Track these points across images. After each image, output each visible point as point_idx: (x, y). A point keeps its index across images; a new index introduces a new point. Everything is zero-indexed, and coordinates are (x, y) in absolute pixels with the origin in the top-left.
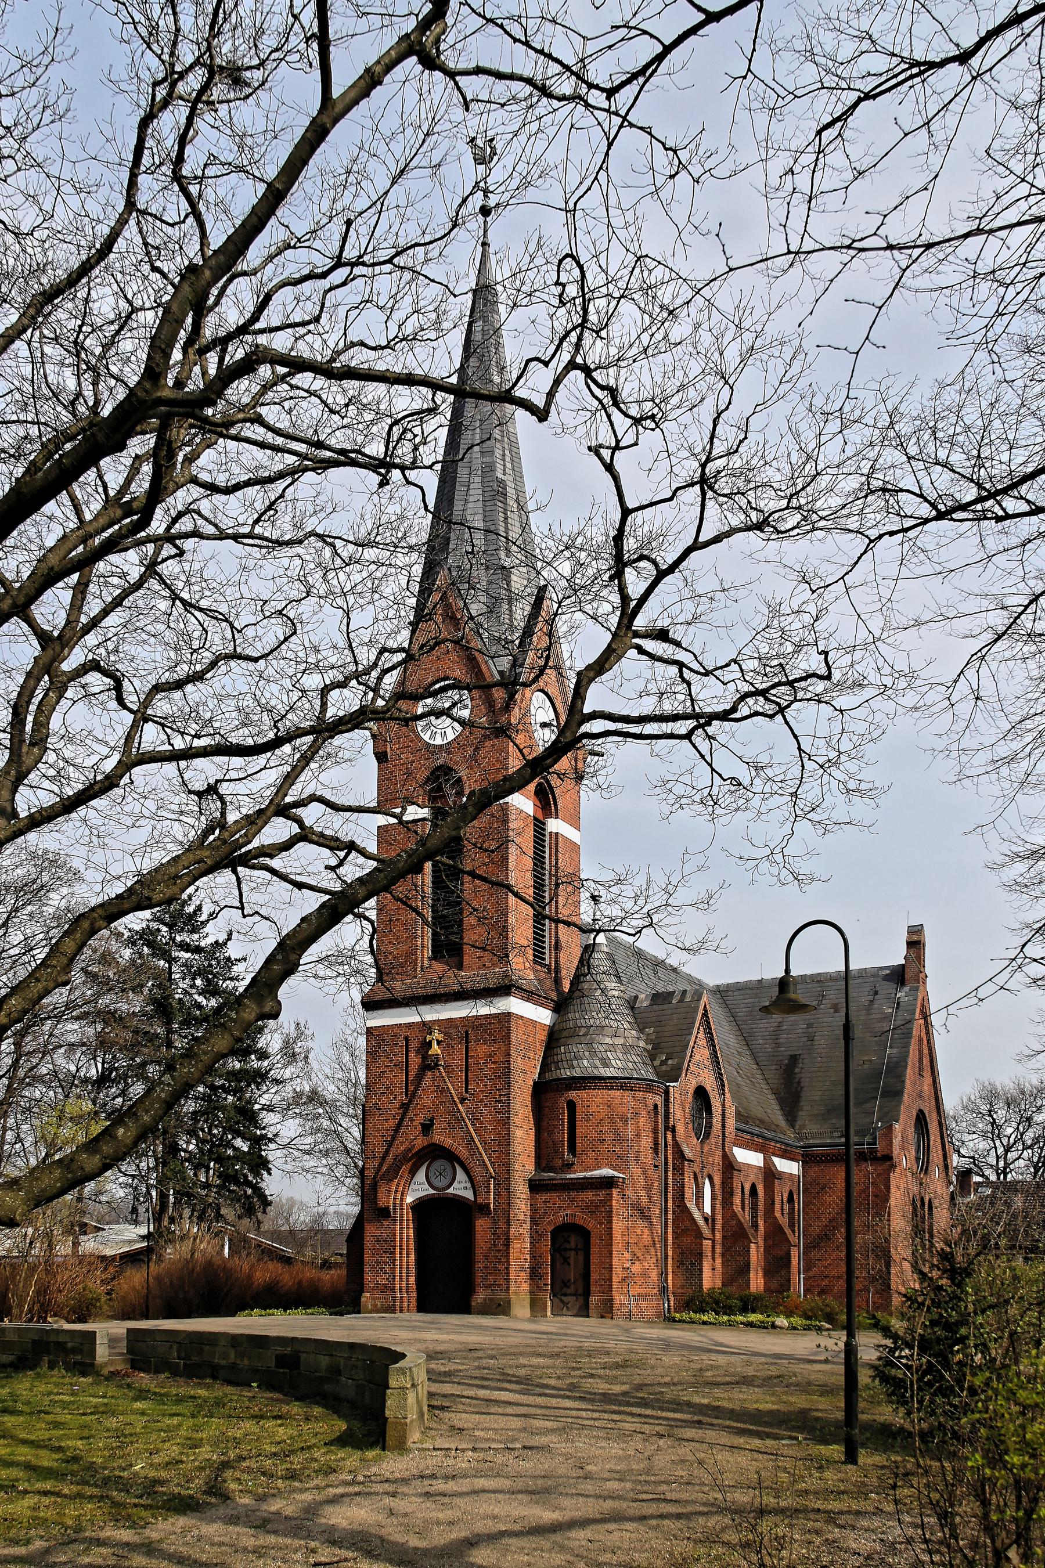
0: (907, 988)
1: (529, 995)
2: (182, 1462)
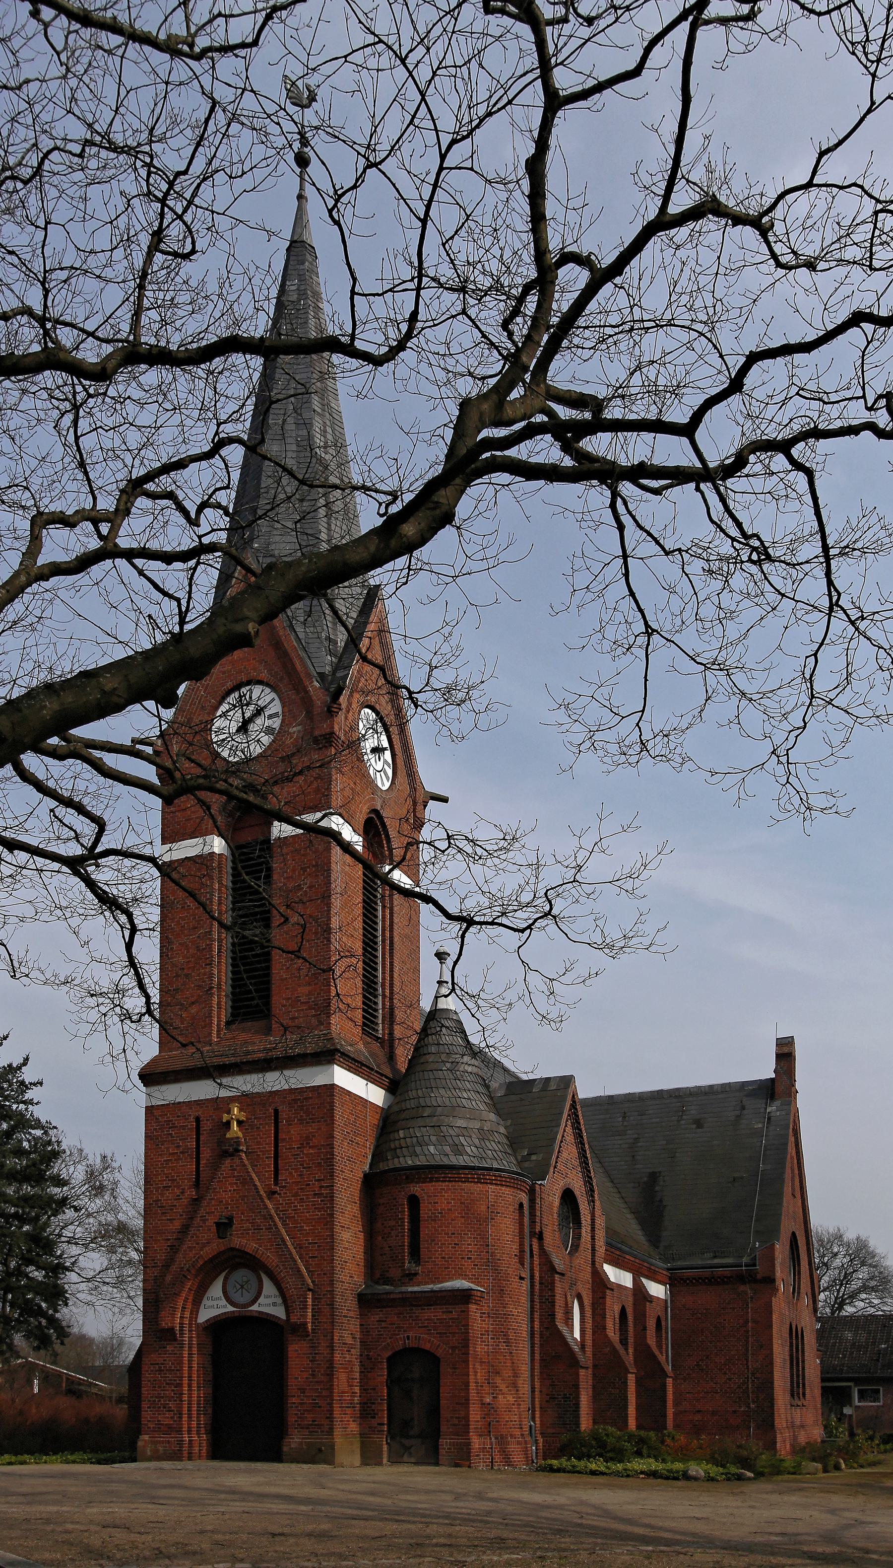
0: (778, 1103)
1: (357, 1067)
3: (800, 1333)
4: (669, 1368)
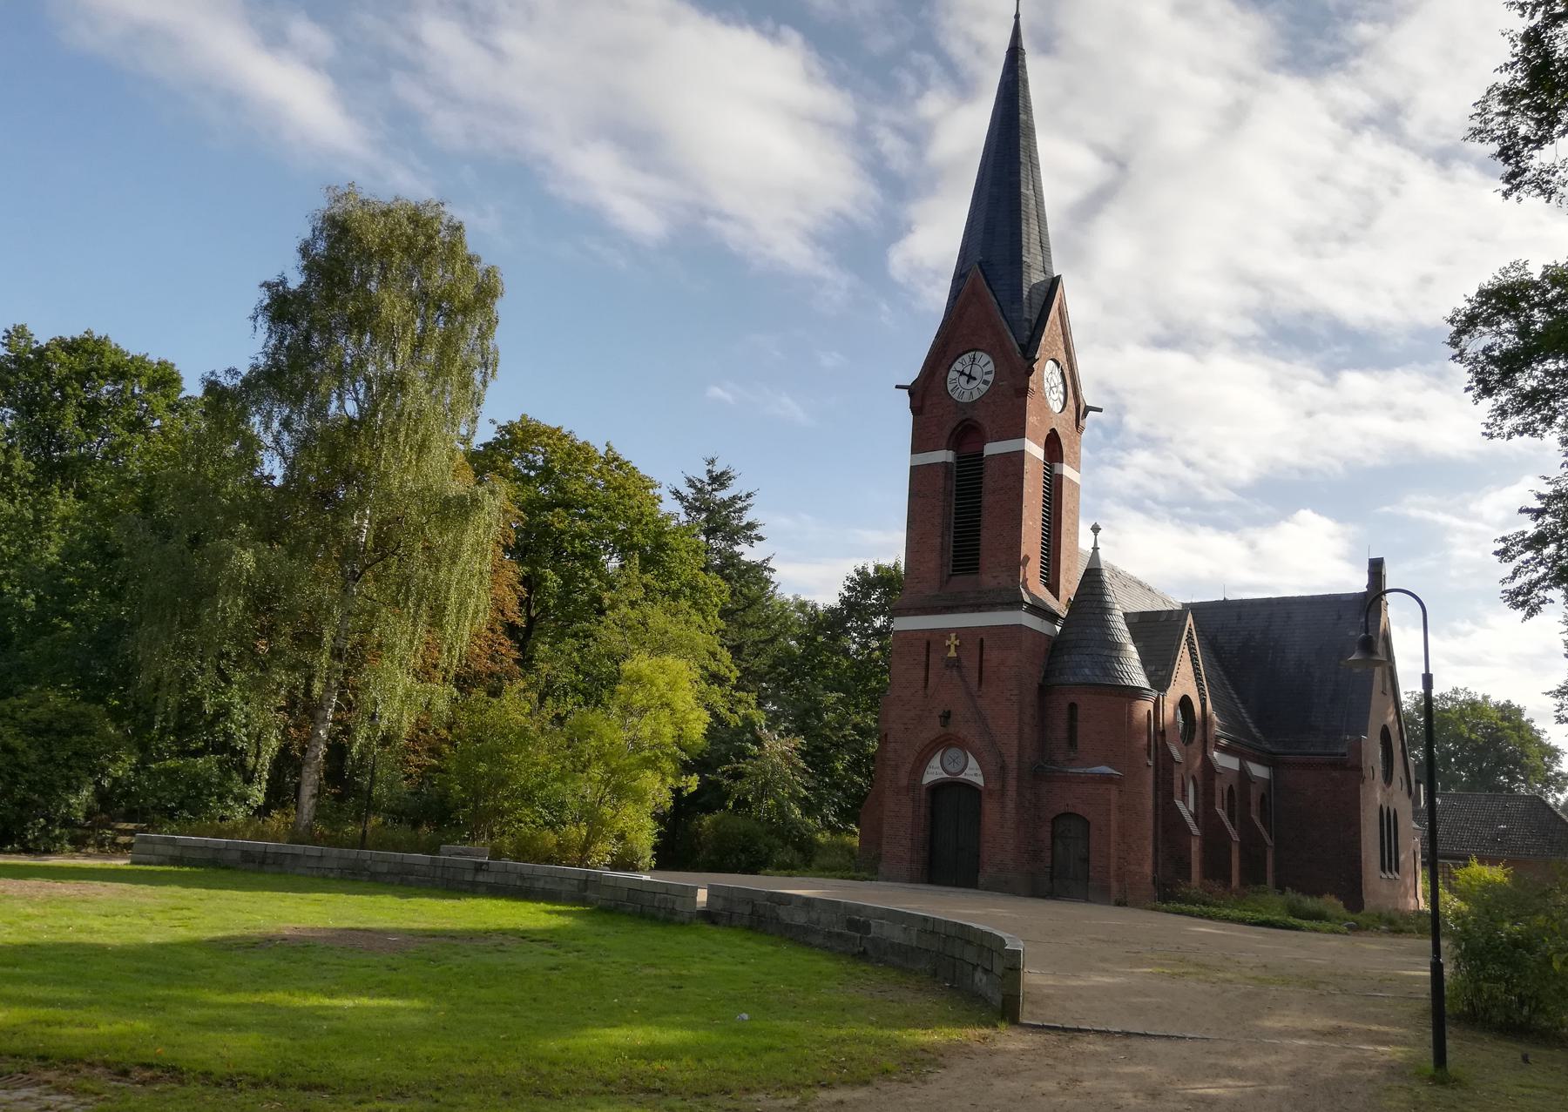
3: (1392, 815)
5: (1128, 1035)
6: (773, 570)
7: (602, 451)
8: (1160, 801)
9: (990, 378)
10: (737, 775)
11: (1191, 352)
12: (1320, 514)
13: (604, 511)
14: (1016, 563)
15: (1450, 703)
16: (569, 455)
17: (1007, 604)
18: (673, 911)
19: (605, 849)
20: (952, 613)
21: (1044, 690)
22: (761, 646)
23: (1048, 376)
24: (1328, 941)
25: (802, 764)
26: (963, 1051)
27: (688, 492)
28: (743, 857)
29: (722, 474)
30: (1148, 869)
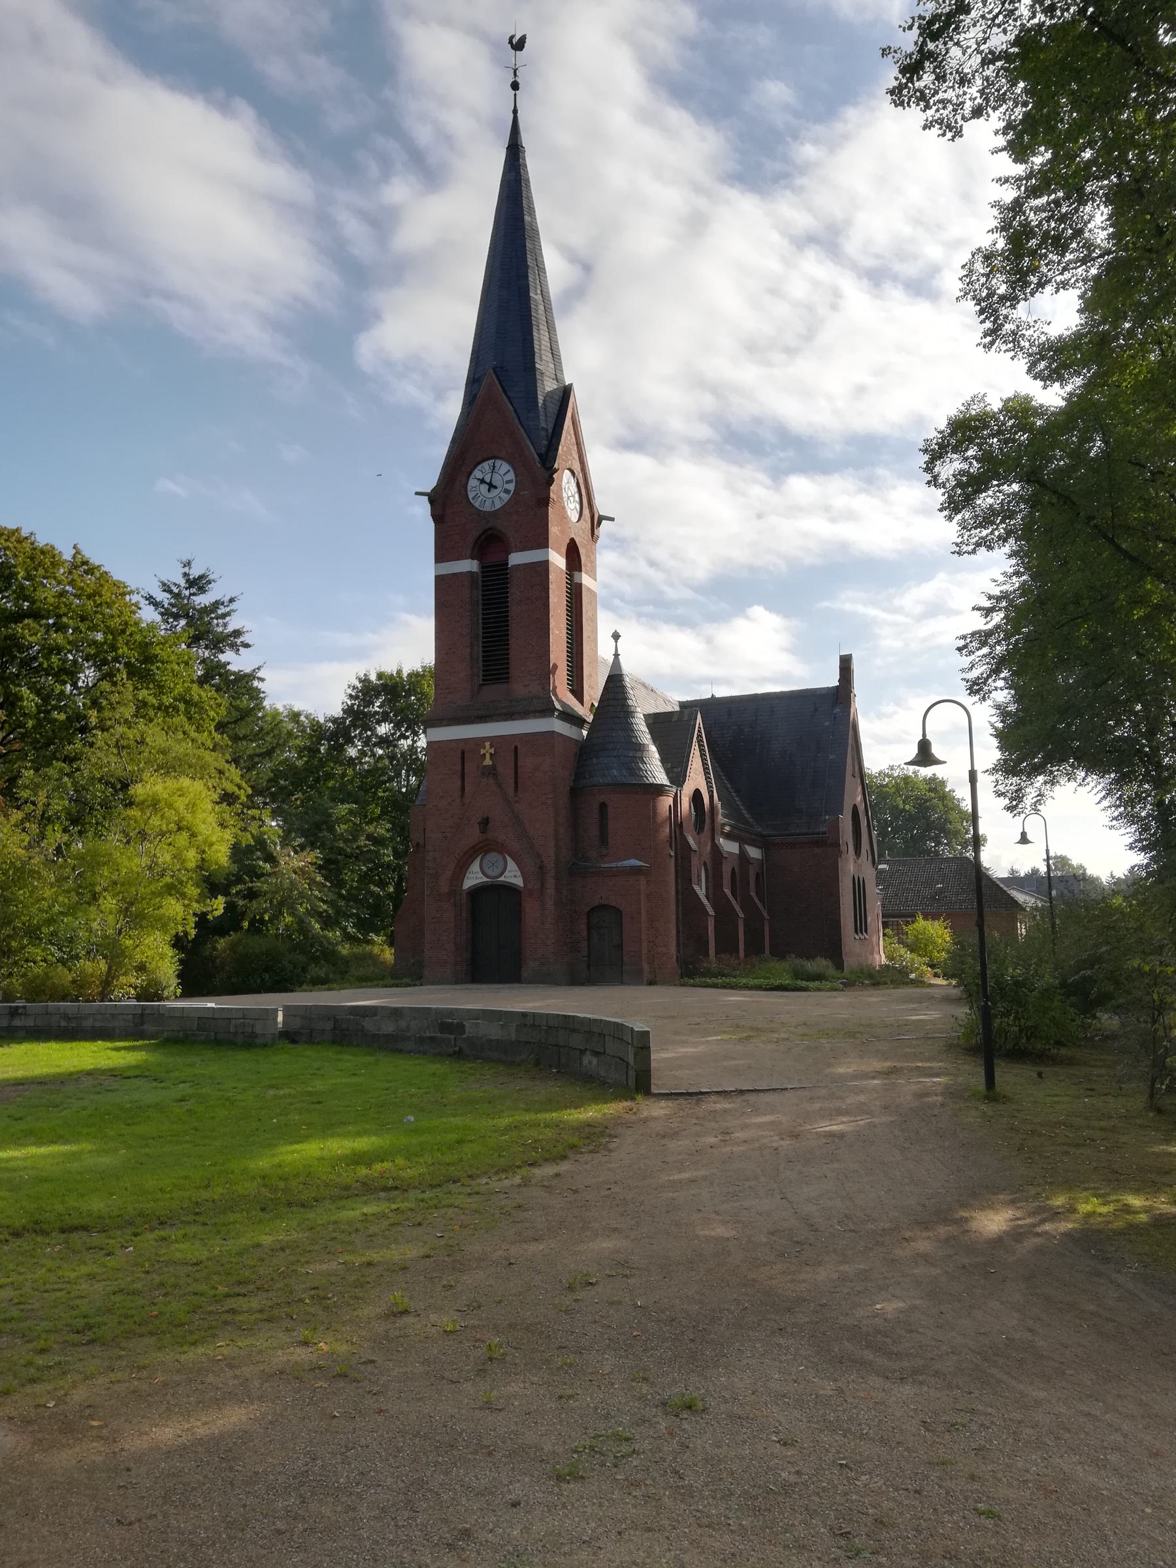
2: (311, 1075)
4: (765, 914)
5: (741, 1092)
6: (262, 680)
7: (68, 555)
8: (680, 887)
9: (511, 487)
10: (252, 895)
11: (654, 455)
12: (770, 612)
13: (81, 621)
14: (546, 671)
15: (887, 780)
16: (32, 559)
17: (539, 712)
18: (253, 1035)
19: (130, 981)
20: (492, 721)
21: (575, 792)
22: (256, 759)
23: (566, 485)
24: (835, 997)
25: (319, 878)
26: (617, 1121)
27: (163, 597)
28: (267, 976)
29: (201, 577)
30: (673, 950)
